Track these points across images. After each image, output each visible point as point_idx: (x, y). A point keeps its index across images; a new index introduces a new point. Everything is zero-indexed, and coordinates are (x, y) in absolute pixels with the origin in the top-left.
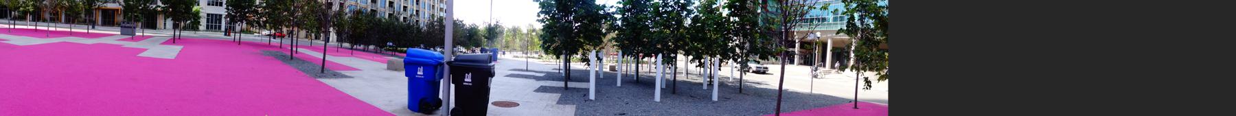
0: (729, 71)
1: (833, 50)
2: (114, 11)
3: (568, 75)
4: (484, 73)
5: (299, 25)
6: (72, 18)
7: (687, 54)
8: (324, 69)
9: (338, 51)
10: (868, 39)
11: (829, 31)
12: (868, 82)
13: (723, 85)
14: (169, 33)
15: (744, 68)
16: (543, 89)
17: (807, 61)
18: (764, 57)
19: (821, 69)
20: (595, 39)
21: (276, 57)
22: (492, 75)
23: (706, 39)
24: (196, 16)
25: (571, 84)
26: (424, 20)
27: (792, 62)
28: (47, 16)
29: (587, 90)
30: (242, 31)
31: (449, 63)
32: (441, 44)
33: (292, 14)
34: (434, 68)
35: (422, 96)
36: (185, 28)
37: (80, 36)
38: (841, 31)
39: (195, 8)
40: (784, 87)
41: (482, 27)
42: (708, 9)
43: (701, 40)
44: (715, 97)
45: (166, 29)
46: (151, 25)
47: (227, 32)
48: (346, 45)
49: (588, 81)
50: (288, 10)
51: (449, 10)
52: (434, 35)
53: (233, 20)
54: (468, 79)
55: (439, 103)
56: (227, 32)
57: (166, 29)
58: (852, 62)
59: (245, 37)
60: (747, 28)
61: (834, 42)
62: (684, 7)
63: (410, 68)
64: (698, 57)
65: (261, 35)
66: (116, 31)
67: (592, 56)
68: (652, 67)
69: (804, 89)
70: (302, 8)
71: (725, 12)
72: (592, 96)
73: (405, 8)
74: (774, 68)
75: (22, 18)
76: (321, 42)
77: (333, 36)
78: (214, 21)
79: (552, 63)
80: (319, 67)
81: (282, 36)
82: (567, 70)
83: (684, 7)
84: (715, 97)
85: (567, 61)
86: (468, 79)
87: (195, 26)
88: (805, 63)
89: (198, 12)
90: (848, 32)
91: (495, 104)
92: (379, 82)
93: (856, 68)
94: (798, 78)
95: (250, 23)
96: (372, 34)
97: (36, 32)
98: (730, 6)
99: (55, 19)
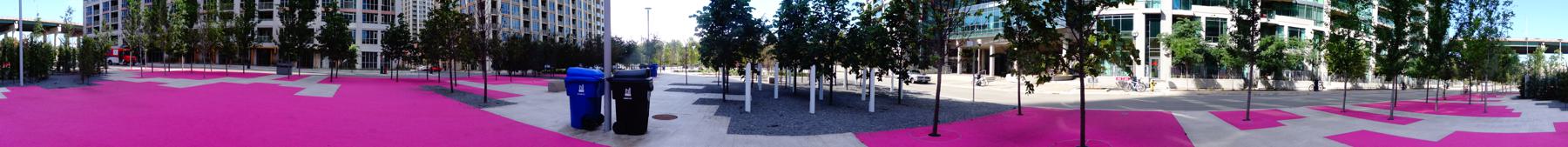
0: (890, 82)
2: (269, 50)
3: (726, 88)
4: (642, 85)
5: (455, 56)
7: (845, 66)
9: (497, 79)
10: (1026, 42)
12: (1030, 86)
15: (904, 77)
16: (702, 102)
17: (968, 70)
18: (925, 66)
19: (984, 77)
22: (651, 89)
23: (866, 47)
24: (353, 54)
25: (728, 97)
26: (581, 39)
27: (955, 71)
30: (398, 68)
31: (609, 79)
32: (601, 63)
33: (448, 46)
34: (595, 86)
35: (585, 117)
36: (341, 67)
37: (237, 76)
40: (1087, 99)
41: (640, 43)
42: (866, 18)
43: (860, 51)
44: (872, 109)
45: (322, 69)
46: (308, 64)
47: (383, 70)
48: (504, 72)
49: (743, 93)
51: (607, 28)
52: (593, 52)
53: (388, 56)
54: (628, 94)
55: (601, 118)
56: (383, 70)
57: (322, 69)
59: (402, 74)
60: (909, 34)
61: (996, 49)
62: (839, 18)
63: (571, 88)
64: (856, 70)
65: (418, 71)
66: (272, 71)
67: (748, 68)
68: (806, 79)
69: (966, 98)
72: (748, 108)
73: (561, 29)
75: (175, 60)
76: (478, 72)
77: (489, 63)
78: (369, 59)
79: (711, 76)
80: (481, 98)
81: (439, 70)
82: (725, 81)
84: (872, 109)
85: (726, 74)
86: (628, 94)
87: (351, 65)
89: (354, 51)
90: (1006, 37)
92: (541, 105)
94: (957, 86)
96: (531, 57)
97: (191, 75)
99: (209, 60)
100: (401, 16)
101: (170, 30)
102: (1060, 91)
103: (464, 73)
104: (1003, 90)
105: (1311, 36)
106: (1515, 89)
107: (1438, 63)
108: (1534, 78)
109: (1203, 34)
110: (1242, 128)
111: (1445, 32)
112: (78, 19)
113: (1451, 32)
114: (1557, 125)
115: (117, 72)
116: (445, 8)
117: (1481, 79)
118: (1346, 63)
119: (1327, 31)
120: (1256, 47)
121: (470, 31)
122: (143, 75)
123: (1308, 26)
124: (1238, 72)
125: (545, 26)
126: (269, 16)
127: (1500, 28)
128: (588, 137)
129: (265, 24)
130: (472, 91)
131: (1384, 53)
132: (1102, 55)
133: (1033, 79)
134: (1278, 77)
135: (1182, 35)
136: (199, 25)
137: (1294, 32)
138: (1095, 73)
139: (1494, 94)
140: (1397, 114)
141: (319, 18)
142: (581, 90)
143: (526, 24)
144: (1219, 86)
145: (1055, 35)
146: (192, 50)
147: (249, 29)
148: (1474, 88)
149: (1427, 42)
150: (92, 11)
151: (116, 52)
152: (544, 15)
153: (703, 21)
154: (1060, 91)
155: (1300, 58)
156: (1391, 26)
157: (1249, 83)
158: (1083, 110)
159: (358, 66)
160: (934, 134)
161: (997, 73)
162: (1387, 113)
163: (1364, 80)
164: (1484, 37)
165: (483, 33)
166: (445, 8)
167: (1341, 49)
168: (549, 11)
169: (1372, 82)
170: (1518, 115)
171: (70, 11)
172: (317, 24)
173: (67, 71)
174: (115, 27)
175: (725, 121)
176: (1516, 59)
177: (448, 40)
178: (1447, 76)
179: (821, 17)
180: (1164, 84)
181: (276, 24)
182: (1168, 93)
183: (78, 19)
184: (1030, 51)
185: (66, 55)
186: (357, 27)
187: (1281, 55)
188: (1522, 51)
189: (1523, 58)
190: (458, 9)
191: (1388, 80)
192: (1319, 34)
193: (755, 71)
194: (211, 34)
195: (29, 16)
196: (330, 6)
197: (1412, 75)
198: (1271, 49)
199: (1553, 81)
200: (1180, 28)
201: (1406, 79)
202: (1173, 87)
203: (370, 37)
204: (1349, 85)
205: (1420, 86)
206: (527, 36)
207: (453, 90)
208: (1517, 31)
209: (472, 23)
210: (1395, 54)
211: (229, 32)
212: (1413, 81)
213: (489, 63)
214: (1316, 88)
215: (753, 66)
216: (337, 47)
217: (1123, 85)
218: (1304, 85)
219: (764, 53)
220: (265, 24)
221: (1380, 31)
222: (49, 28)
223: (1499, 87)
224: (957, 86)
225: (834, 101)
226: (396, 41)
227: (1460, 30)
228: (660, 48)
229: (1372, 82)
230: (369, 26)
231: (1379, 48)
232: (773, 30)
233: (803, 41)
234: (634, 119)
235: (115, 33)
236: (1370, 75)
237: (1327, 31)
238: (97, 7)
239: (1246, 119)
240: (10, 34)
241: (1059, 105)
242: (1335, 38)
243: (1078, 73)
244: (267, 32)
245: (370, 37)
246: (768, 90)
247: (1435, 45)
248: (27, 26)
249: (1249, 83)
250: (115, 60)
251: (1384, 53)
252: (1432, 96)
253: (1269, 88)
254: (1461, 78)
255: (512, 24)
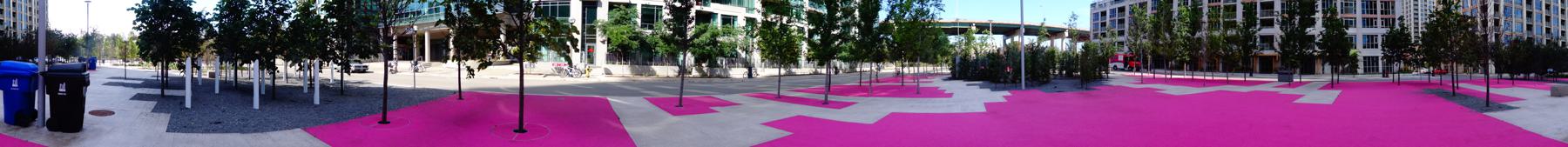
0: (330, 73)
1: (431, 41)
3: (165, 83)
4: (78, 82)
5: (1458, 59)
6: (1230, 68)
7: (287, 60)
8: (1489, 103)
9: (1499, 82)
11: (427, 21)
12: (470, 70)
13: (324, 87)
14: (1327, 78)
15: (346, 68)
16: (139, 97)
17: (406, 56)
19: (421, 63)
20: (193, 46)
21: (1439, 95)
22: (88, 84)
23: (305, 41)
25: (167, 92)
26: (21, 32)
28: (1205, 66)
29: (183, 98)
30: (1400, 71)
34: (29, 80)
36: (1344, 72)
37: (1237, 85)
38: (439, 22)
39: (1352, 52)
40: (526, 84)
41: (79, 36)
42: (305, 10)
44: (317, 101)
45: (1325, 74)
47: (1385, 74)
48: (1506, 75)
49: (183, 87)
50: (1445, 45)
53: (1389, 60)
54: (62, 89)
56: (1385, 74)
58: (452, 54)
59: (1404, 77)
61: (432, 35)
62: (280, 11)
65: (1420, 74)
66: (1274, 78)
68: (250, 72)
70: (1458, 43)
71: (323, 14)
72: (188, 104)
74: (376, 67)
75: (1179, 68)
76: (1480, 76)
77: (1492, 68)
78: (1371, 63)
79: (150, 70)
81: (1442, 73)
83: (280, 11)
84: (317, 101)
86: (62, 89)
87: (1353, 70)
88: (404, 59)
89: (1355, 56)
90: (446, 22)
91: (92, 113)
93: (457, 58)
94: (404, 75)
95: (1407, 63)
98: (327, 8)
99: (1212, 68)
100: (1401, 18)
101: (1173, 37)
102: (500, 76)
103: (1466, 76)
104: (442, 76)
105: (744, 23)
106: (946, 70)
107: (870, 47)
108: (965, 58)
109: (639, 21)
110: (675, 113)
111: (876, 15)
112: (1084, 24)
113: (882, 15)
114: (988, 105)
115: (1119, 77)
116: (1447, 10)
117: (913, 61)
118: (780, 49)
119: (759, 18)
120: (690, 34)
121: (1473, 34)
122: (1143, 80)
123: (740, 13)
124: (672, 58)
125: (1548, 30)
126: (1269, 23)
127: (932, 10)
128: (21, 134)
129: (1266, 31)
130: (1475, 94)
131: (817, 38)
132: (539, 42)
133: (473, 64)
134: (713, 65)
135: (617, 22)
136: (1202, 34)
137: (728, 20)
138: (533, 59)
139: (926, 75)
140: (831, 98)
141: (1319, 23)
142: (15, 85)
143: (1530, 27)
144: (653, 73)
145: (495, 21)
146: (1196, 58)
147: (1249, 37)
148: (906, 70)
149: (859, 26)
150: (1098, 16)
151: (1121, 58)
152: (1548, 19)
153: (142, 14)
154: (500, 76)
155: (733, 46)
156: (824, 11)
157: (683, 71)
158: (521, 97)
159: (1360, 71)
160: (384, 121)
161: (433, 59)
162: (822, 97)
163: (797, 65)
164: (915, 19)
165: (1485, 36)
166: (1447, 10)
167: (774, 35)
168: (1535, 11)
169: (805, 68)
170: (950, 95)
171: (1074, 17)
172: (1317, 30)
173: (1069, 75)
174: (1121, 33)
175: (164, 118)
176: (947, 41)
177: (1450, 42)
178: (879, 58)
179: (261, 10)
180: (599, 70)
181: (1276, 31)
182: (605, 79)
183: (1084, 24)
184: (473, 40)
185: (1069, 62)
186: (1357, 32)
187: (715, 43)
188: (954, 32)
189: (952, 39)
190: (1461, 11)
191: (821, 65)
192: (750, 21)
193: (195, 66)
194: (1213, 42)
195: (1032, 20)
196: (1329, 10)
197: (845, 60)
198: (704, 38)
199: (983, 62)
200: (617, 15)
201: (838, 63)
202: (608, 73)
203: (1370, 42)
204: (783, 71)
205: (852, 69)
206: (1530, 40)
207: (1454, 93)
208: (948, 14)
209: (1474, 25)
210: (827, 39)
211: (1230, 40)
212: (845, 66)
213: (1492, 68)
214: (750, 75)
215: (193, 60)
216: (1337, 51)
217: (560, 70)
218: (738, 73)
219: (204, 47)
220: (1266, 31)
221: (813, 17)
222: (1055, 33)
223: (930, 68)
224: (404, 75)
225: (274, 95)
226: (1397, 44)
227: (892, 13)
228: (100, 41)
229: (805, 68)
230: (1370, 31)
231: (811, 33)
232: (214, 23)
233: (243, 36)
234: (69, 117)
235: (1121, 39)
236: (802, 60)
237: (759, 18)
238: (1104, 14)
239: (679, 104)
240: (1016, 38)
241: (498, 89)
242: (767, 25)
243: (518, 58)
244: (1268, 40)
245: (1370, 42)
246: (208, 84)
247: (866, 30)
248: (1030, 31)
249: (683, 71)
250: (1120, 65)
251: (817, 38)
252: (865, 79)
253: (704, 76)
254: (892, 60)
255: (1515, 27)
